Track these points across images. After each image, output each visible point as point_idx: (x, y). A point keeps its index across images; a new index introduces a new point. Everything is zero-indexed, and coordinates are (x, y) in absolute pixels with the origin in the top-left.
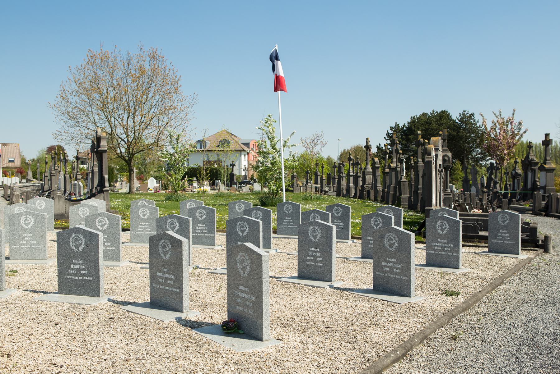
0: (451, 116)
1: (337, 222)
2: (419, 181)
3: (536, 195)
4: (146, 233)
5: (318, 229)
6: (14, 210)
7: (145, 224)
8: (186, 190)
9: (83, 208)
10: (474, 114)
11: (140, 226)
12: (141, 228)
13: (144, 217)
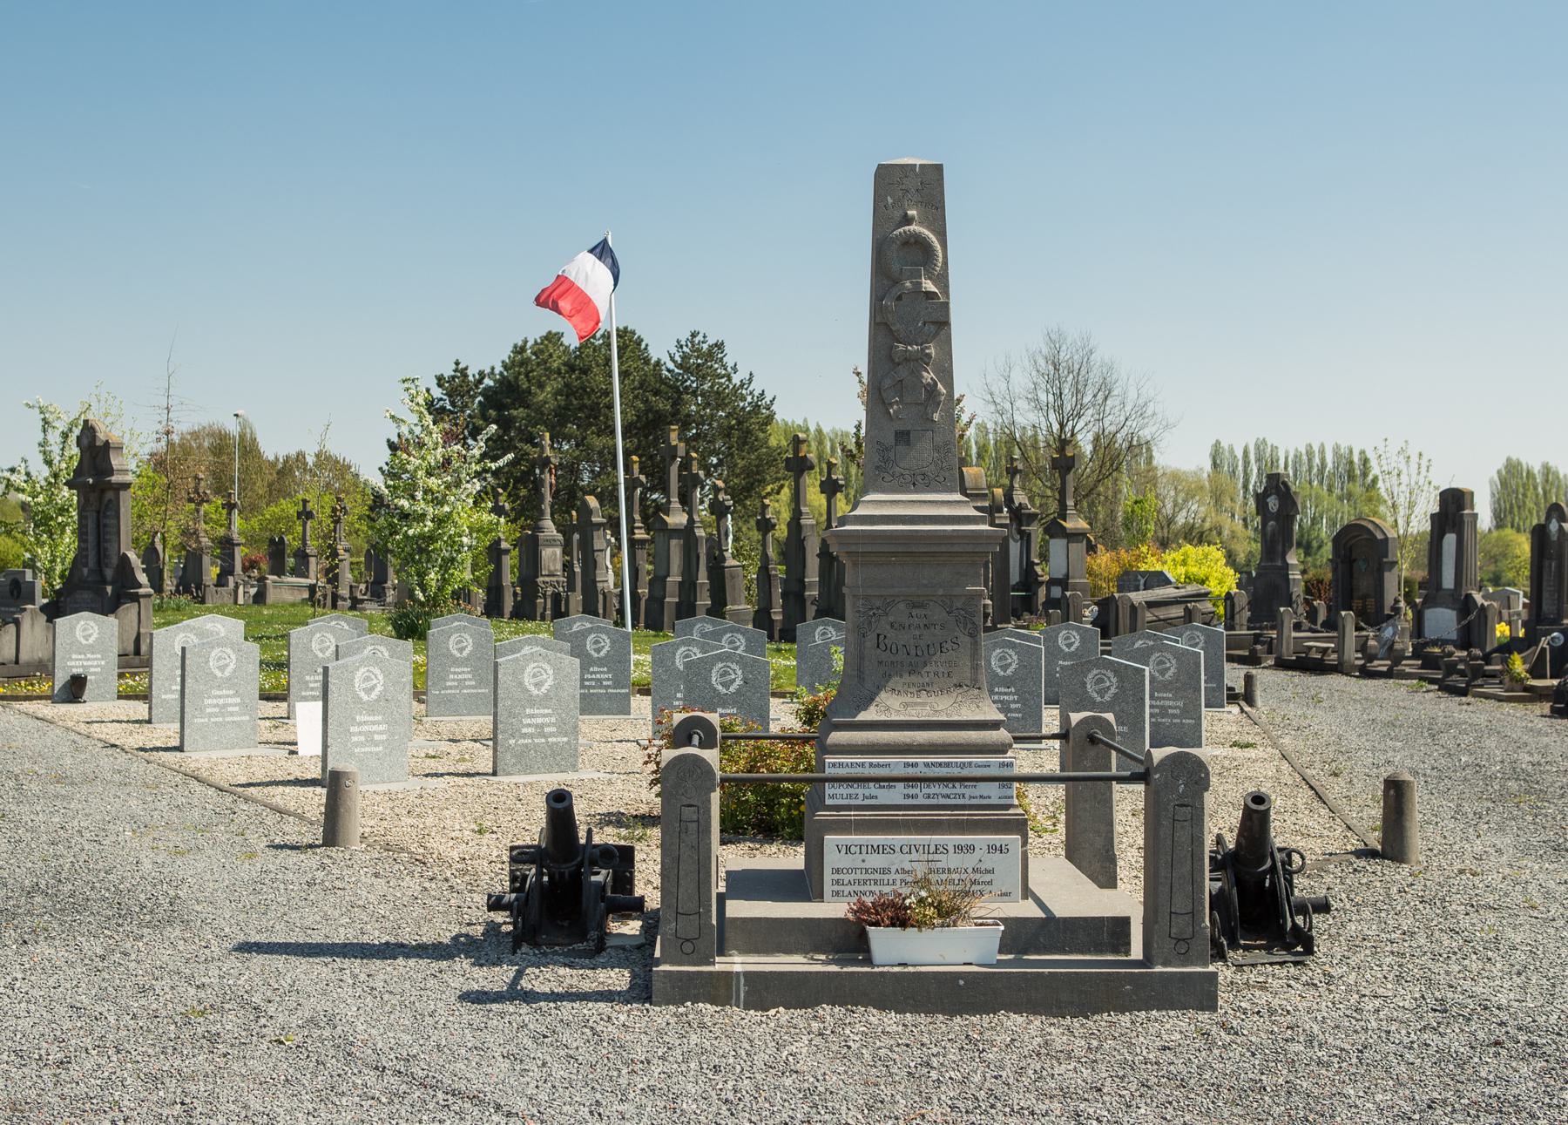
0: (646, 349)
2: (804, 567)
3: (1070, 601)
5: (1013, 654)
6: (174, 641)
8: (1503, 580)
10: (722, 343)
11: (451, 676)
12: (453, 680)
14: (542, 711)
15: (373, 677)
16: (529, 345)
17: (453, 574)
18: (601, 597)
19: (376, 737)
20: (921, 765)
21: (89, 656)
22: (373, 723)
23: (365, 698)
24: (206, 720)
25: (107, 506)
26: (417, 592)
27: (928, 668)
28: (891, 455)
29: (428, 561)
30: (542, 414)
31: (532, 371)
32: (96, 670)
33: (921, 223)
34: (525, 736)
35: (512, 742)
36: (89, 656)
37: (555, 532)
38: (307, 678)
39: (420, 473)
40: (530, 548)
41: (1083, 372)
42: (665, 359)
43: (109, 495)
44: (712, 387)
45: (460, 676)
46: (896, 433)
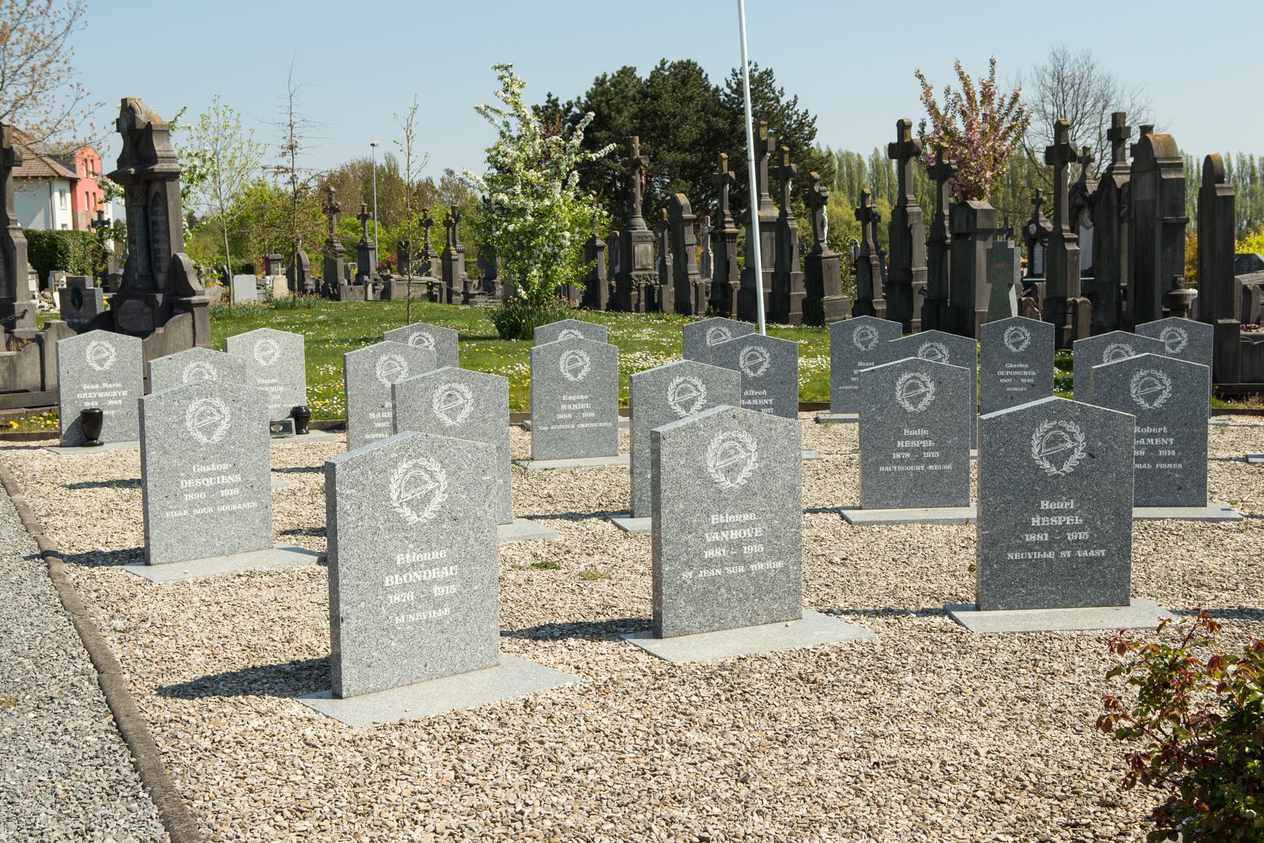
0: (706, 78)
1: (1015, 369)
2: (911, 255)
4: (582, 426)
6: (182, 374)
7: (578, 397)
9: (390, 358)
10: (771, 71)
11: (564, 407)
12: (567, 412)
13: (576, 377)
14: (738, 518)
15: (426, 477)
16: (608, 78)
17: (556, 271)
18: (693, 289)
19: (437, 591)
21: (105, 385)
22: (430, 565)
23: (413, 518)
24: (185, 512)
25: (154, 199)
26: (519, 290)
29: (530, 257)
30: (621, 135)
31: (612, 99)
32: (115, 402)
34: (709, 563)
35: (688, 575)
36: (105, 385)
37: (646, 230)
38: (372, 415)
39: (519, 165)
40: (623, 246)
41: (1083, 86)
42: (723, 85)
43: (156, 187)
44: (763, 108)
45: (575, 406)
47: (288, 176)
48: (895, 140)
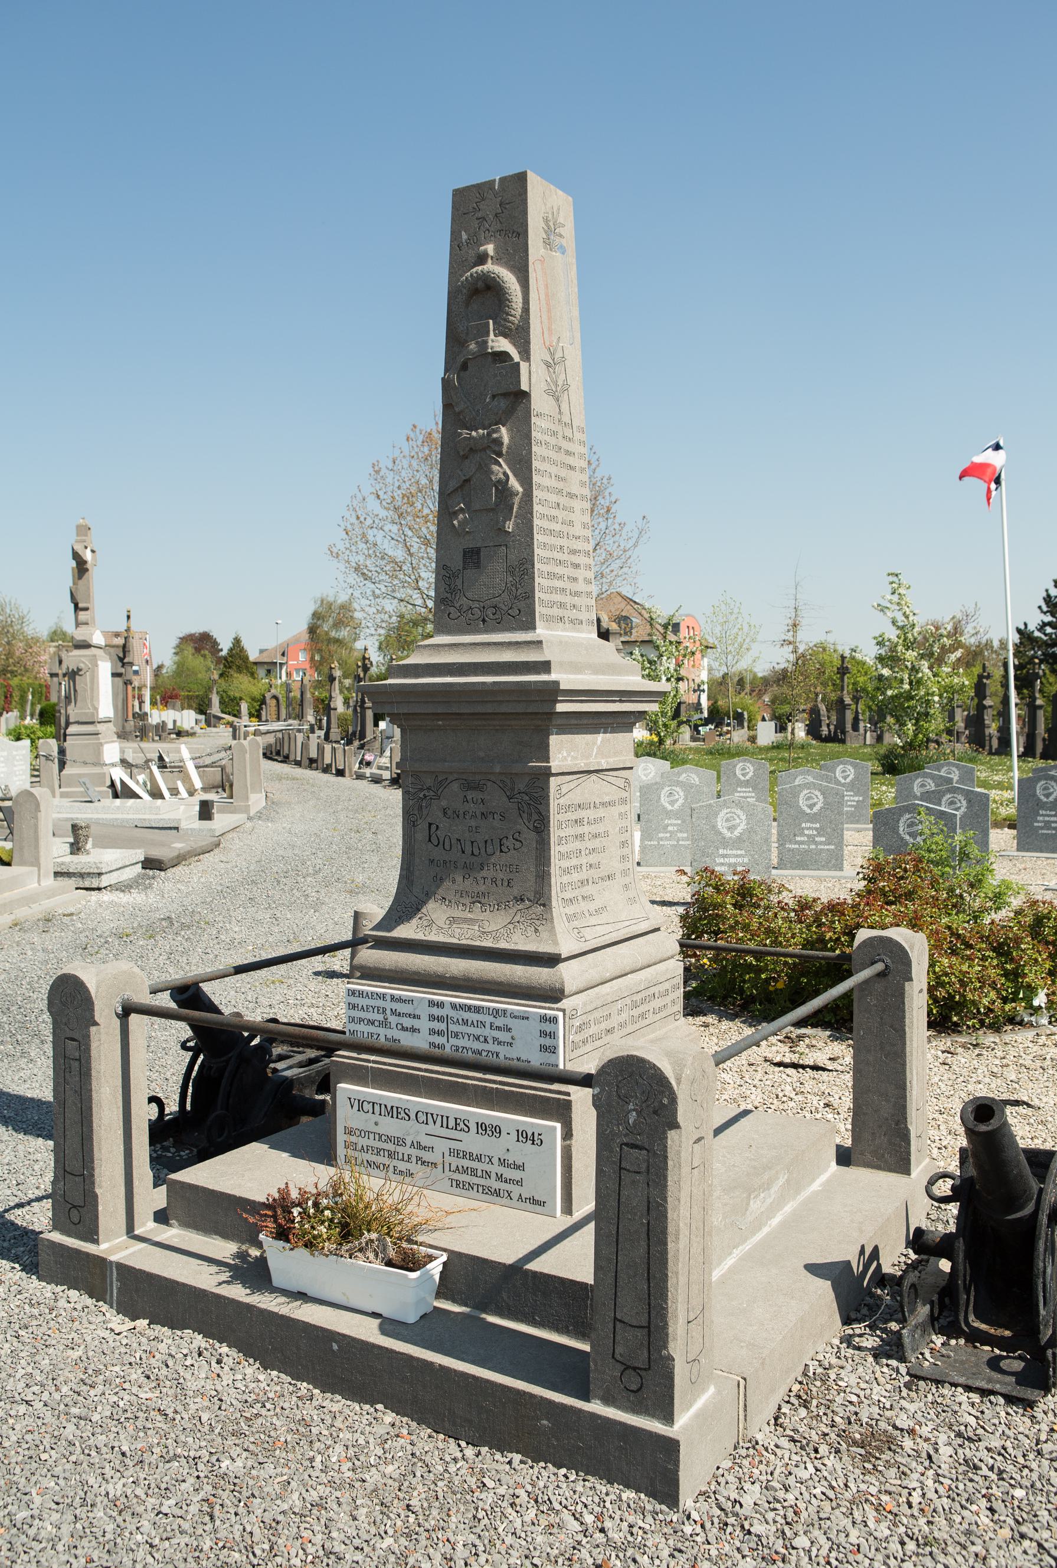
14: (735, 852)
20: (447, 1006)
27: (484, 873)
28: (459, 582)
33: (498, 260)
46: (465, 552)
47: (791, 647)
48: (562, 687)
